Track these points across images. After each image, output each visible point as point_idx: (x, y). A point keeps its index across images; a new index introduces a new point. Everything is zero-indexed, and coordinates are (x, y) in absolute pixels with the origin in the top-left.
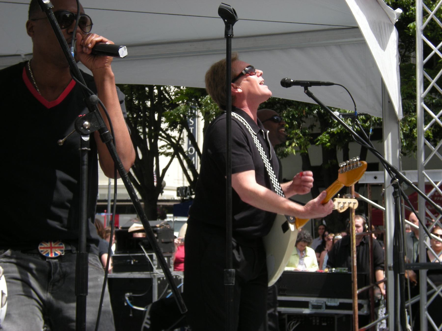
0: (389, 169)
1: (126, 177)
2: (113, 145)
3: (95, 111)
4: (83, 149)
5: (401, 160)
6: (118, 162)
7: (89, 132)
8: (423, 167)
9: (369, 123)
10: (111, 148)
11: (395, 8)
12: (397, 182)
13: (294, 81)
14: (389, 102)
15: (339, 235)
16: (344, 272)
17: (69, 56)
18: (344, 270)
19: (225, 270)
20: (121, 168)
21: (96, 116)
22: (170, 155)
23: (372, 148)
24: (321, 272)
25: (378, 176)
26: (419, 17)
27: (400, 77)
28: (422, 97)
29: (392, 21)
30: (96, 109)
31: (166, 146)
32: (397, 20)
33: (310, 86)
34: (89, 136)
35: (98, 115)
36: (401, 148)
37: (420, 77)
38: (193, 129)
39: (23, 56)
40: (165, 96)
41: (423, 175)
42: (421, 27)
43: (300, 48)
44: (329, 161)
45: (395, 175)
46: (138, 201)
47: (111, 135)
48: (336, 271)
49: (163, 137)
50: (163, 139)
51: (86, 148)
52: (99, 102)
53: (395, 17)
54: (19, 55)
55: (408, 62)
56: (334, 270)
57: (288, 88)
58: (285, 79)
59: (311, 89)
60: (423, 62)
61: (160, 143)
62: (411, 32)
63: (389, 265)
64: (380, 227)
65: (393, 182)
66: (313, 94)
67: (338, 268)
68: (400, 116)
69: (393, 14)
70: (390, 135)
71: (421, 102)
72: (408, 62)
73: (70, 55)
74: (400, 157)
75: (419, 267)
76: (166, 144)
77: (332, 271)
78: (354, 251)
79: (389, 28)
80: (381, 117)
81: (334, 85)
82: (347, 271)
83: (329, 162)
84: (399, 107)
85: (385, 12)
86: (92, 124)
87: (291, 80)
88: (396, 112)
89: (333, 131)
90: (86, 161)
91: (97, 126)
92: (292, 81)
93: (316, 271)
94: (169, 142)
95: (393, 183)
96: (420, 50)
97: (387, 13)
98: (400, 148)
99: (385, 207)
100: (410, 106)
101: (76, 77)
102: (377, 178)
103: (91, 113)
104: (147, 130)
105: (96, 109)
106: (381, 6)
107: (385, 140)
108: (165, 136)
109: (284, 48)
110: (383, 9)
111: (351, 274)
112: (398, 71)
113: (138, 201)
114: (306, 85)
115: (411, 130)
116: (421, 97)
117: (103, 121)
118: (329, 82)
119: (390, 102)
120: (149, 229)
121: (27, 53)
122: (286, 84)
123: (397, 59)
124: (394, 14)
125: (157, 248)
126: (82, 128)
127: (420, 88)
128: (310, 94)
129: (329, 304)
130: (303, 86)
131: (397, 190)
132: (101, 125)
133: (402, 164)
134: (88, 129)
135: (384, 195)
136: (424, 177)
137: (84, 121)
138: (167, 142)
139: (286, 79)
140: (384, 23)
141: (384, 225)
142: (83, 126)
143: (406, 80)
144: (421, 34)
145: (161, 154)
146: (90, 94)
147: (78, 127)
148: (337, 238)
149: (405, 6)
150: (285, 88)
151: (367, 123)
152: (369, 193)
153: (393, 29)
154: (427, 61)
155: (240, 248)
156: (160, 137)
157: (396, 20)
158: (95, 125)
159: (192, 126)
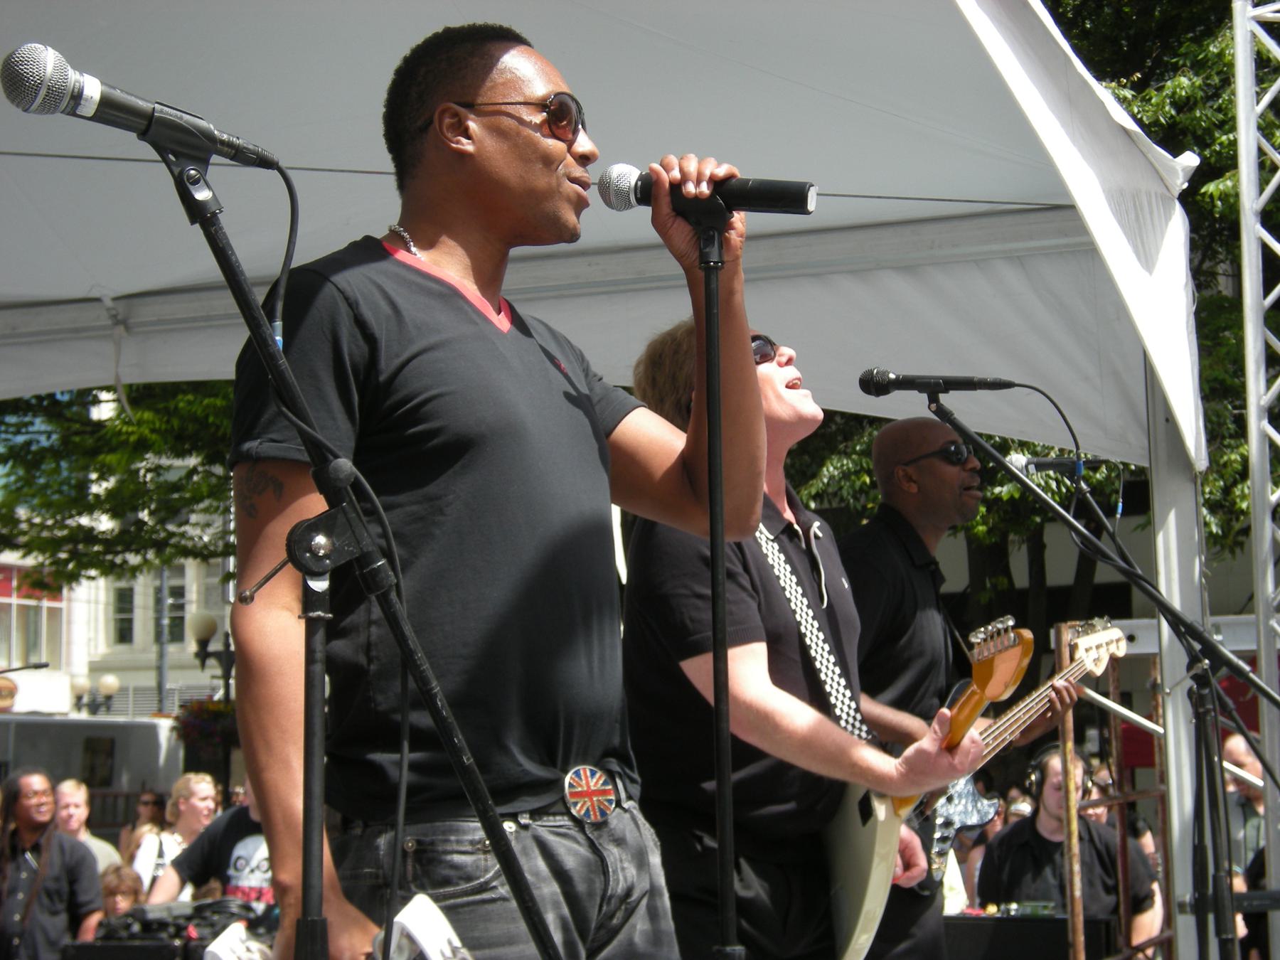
0: (1180, 630)
1: (436, 694)
2: (398, 601)
3: (345, 504)
4: (311, 614)
5: (1205, 588)
6: (411, 650)
7: (327, 565)
8: (1272, 609)
9: (1105, 471)
10: (392, 610)
11: (1176, 152)
12: (1205, 667)
13: (898, 377)
14: (1167, 420)
15: (1023, 801)
16: (1044, 915)
17: (270, 348)
18: (1045, 907)
19: (716, 948)
20: (422, 669)
21: (348, 520)
23: (1132, 569)
24: (977, 915)
25: (1138, 634)
26: (1249, 174)
27: (1198, 343)
28: (1263, 406)
29: (1170, 187)
30: (347, 499)
32: (1186, 185)
33: (946, 391)
34: (328, 576)
35: (354, 515)
36: (1205, 552)
37: (1255, 348)
39: (109, 303)
41: (1273, 634)
42: (1253, 202)
43: (907, 269)
44: (987, 581)
45: (1197, 646)
46: (471, 763)
47: (391, 573)
48: (1020, 912)
51: (320, 613)
52: (356, 485)
53: (1178, 178)
54: (98, 300)
55: (1212, 288)
56: (1014, 910)
57: (882, 397)
58: (873, 372)
59: (949, 400)
60: (1262, 304)
62: (1219, 208)
63: (1180, 899)
64: (1141, 773)
65: (1195, 668)
66: (953, 414)
67: (1027, 904)
68: (1201, 460)
69: (1173, 171)
70: (1172, 517)
71: (1260, 419)
72: (1212, 288)
73: (271, 345)
74: (1203, 580)
75: (1267, 902)
77: (1008, 911)
78: (1075, 855)
79: (1162, 210)
80: (1146, 465)
81: (1016, 388)
82: (1052, 913)
83: (988, 585)
84: (1198, 434)
85: (1151, 164)
86: (335, 542)
87: (889, 373)
88: (1188, 449)
89: (1001, 492)
90: (320, 651)
91: (351, 549)
92: (892, 376)
93: (962, 913)
95: (1193, 672)
96: (1254, 271)
97: (1157, 165)
98: (1202, 553)
99: (1164, 726)
100: (1222, 420)
101: (288, 408)
102: (1135, 642)
103: (332, 510)
105: (347, 499)
106: (1138, 147)
107: (1158, 532)
109: (862, 270)
110: (1144, 155)
111: (1064, 921)
112: (1190, 329)
113: (469, 762)
114: (933, 388)
115: (1227, 491)
116: (1258, 405)
117: (367, 532)
118: (1001, 379)
119: (1170, 420)
120: (503, 843)
121: (119, 294)
122: (873, 385)
123: (1187, 297)
124: (1177, 170)
125: (527, 898)
126: (308, 555)
127: (1257, 379)
128: (942, 413)
130: (925, 393)
131: (1206, 691)
132: (361, 546)
133: (1210, 601)
134: (326, 556)
135: (1156, 688)
136: (1274, 637)
139: (875, 371)
140: (1149, 194)
141: (1158, 767)
142: (310, 549)
143: (1209, 343)
144: (1255, 224)
147: (297, 553)
148: (1016, 810)
149: (1200, 132)
150: (873, 397)
151: (1100, 471)
152: (1113, 681)
153: (1174, 209)
154: (1275, 299)
155: (743, 862)
157: (1183, 184)
158: (346, 545)
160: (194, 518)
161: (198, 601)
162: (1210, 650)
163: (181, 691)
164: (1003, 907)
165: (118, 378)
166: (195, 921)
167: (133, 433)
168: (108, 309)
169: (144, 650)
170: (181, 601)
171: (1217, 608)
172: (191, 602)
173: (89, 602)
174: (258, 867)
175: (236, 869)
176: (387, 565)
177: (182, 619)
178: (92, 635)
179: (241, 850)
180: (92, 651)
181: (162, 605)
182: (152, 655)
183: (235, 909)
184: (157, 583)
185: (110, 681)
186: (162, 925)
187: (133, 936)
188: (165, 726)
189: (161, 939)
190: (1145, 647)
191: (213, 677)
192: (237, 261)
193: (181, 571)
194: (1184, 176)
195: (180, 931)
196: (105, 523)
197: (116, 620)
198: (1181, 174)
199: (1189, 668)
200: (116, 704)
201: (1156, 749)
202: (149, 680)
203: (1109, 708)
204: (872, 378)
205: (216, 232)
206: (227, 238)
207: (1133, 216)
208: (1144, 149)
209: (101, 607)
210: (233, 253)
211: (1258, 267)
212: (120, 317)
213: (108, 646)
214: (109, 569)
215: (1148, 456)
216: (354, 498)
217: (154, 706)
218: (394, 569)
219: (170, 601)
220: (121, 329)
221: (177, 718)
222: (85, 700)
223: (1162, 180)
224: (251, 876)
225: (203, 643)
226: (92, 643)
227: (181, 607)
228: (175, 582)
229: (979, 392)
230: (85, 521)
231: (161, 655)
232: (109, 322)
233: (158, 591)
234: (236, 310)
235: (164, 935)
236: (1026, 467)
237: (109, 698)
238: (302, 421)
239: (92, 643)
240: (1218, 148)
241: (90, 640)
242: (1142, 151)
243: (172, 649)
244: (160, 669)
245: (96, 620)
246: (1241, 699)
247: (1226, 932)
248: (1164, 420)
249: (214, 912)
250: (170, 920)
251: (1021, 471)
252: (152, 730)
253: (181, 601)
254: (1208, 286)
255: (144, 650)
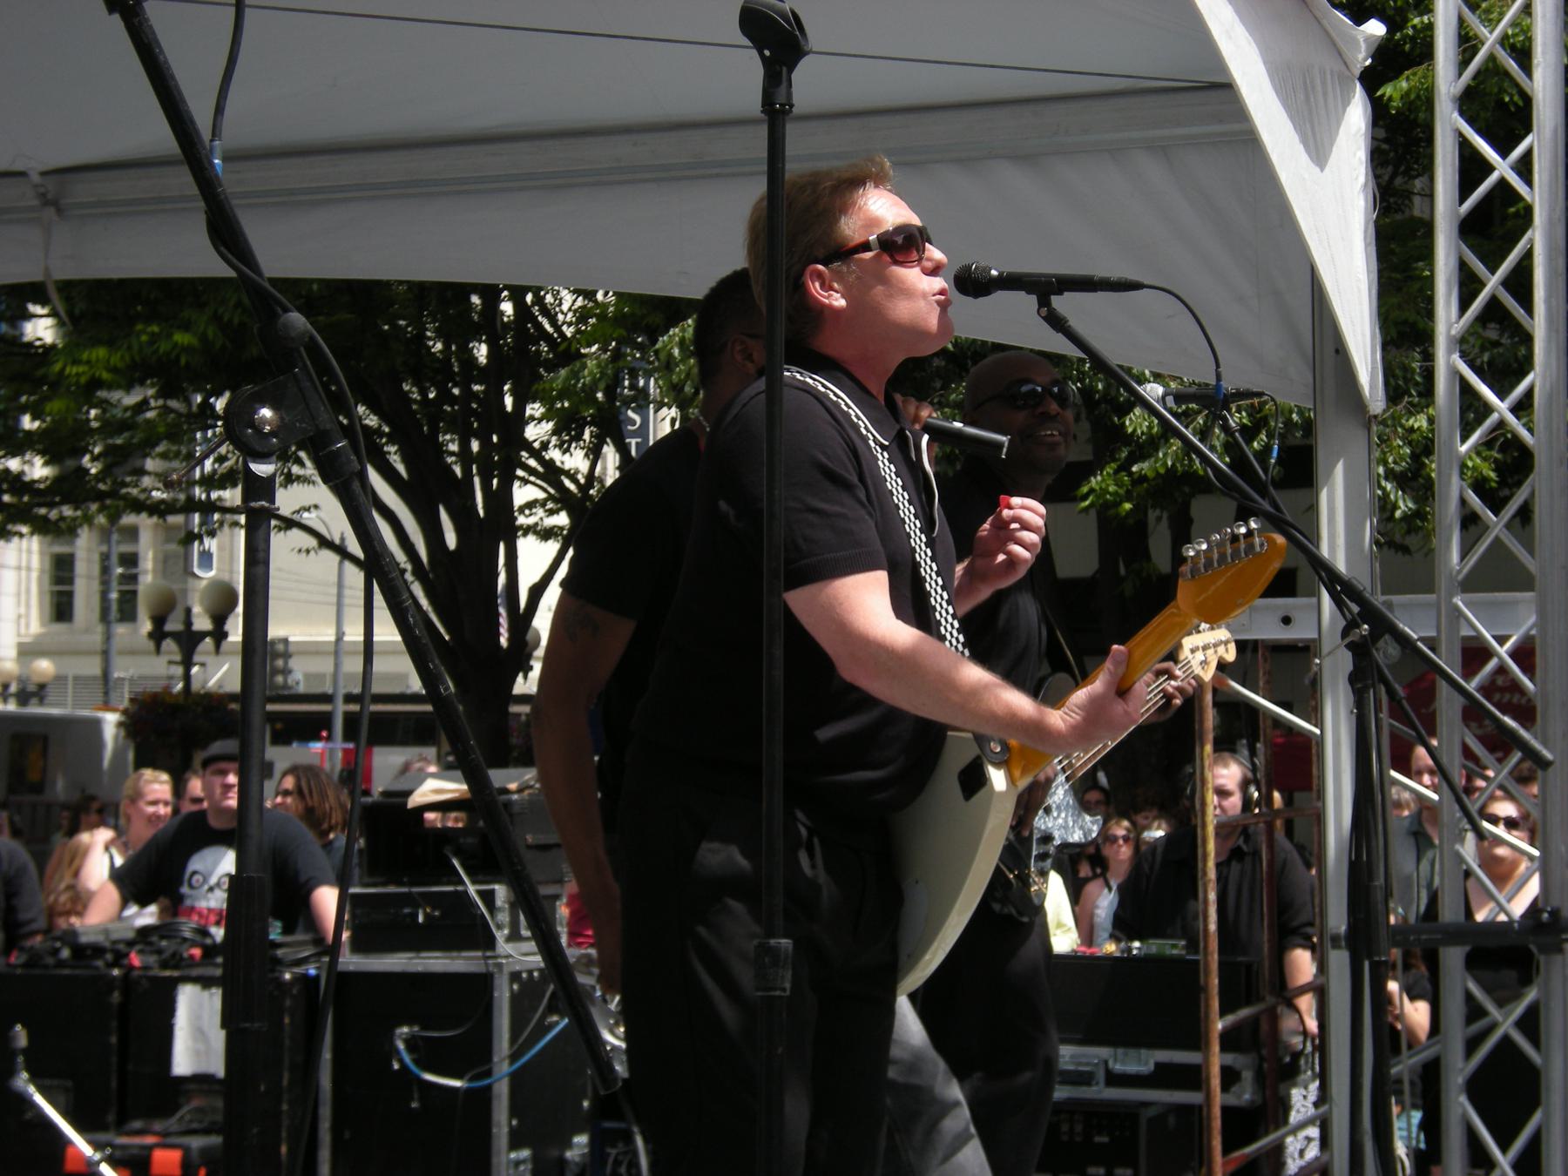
4: (253, 504)
5: (1376, 557)
7: (274, 445)
9: (1265, 439)
11: (1359, 19)
13: (1001, 274)
14: (1337, 351)
18: (1174, 946)
22: (556, 535)
25: (1293, 614)
26: (1446, 50)
28: (1454, 336)
30: (300, 364)
31: (543, 504)
33: (1060, 292)
35: (308, 384)
38: (637, 443)
39: (36, 178)
40: (539, 326)
43: (1024, 158)
45: (1355, 609)
47: (353, 457)
49: (532, 471)
50: (532, 479)
52: (312, 347)
53: (1360, 52)
54: (22, 174)
60: (1457, 212)
61: (523, 494)
63: (1334, 931)
69: (1355, 41)
71: (1450, 352)
76: (541, 495)
77: (1130, 950)
78: (1210, 880)
82: (1184, 952)
86: (284, 416)
91: (304, 425)
92: (994, 272)
93: (1073, 951)
94: (552, 491)
95: (1347, 640)
96: (1449, 170)
97: (1334, 35)
104: (475, 446)
105: (300, 364)
107: (1323, 488)
108: (540, 469)
111: (1197, 962)
114: (1045, 288)
125: (516, 860)
127: (1448, 303)
128: (1056, 322)
129: (1118, 1067)
134: (272, 434)
135: (1315, 683)
136: (1458, 617)
137: (257, 406)
138: (545, 490)
145: (525, 535)
146: (279, 310)
152: (1264, 674)
156: (520, 473)
157: (1366, 60)
159: (634, 434)
160: (150, 464)
161: (155, 571)
162: (1383, 626)
163: (131, 680)
164: (1123, 945)
165: (47, 271)
166: (138, 947)
167: (83, 373)
168: (36, 186)
169: (87, 631)
170: (134, 571)
171: (1391, 586)
172: (146, 572)
173: (19, 568)
174: (218, 885)
175: (191, 886)
176: (349, 448)
177: (134, 593)
178: (23, 610)
179: (197, 863)
180: (23, 631)
181: (110, 576)
182: (96, 638)
183: (188, 934)
184: (104, 548)
185: (45, 666)
186: (98, 950)
187: (61, 964)
188: (111, 720)
189: (97, 968)
190: (1300, 632)
191: (170, 662)
192: (166, 62)
193: (132, 533)
194: (1367, 48)
195: (119, 958)
196: (38, 470)
197: (52, 593)
198: (1363, 46)
199: (1345, 633)
200: (51, 695)
201: (1314, 759)
202: (93, 667)
203: (1258, 703)
204: (970, 275)
205: (141, 24)
206: (154, 33)
207: (1301, 96)
208: (1318, 14)
209: (35, 575)
210: (161, 51)
211: (1454, 164)
212: (50, 196)
213: (43, 624)
214: (42, 527)
215: (1312, 396)
216: (308, 363)
217: (100, 698)
218: (357, 452)
219: (120, 570)
220: (51, 211)
221: (125, 712)
222: (13, 688)
223: (1340, 54)
224: (210, 895)
225: (159, 620)
226: (23, 621)
227: (133, 579)
228: (126, 548)
229: (1100, 294)
230: (14, 464)
231: (108, 637)
232: (35, 202)
233: (105, 558)
234: (195, 191)
235: (100, 963)
236: (1164, 397)
237: (42, 687)
238: (246, 266)
239: (23, 621)
240: (1410, 32)
241: (19, 617)
242: (1315, 17)
243: (121, 630)
244: (106, 654)
245: (28, 591)
246: (1423, 711)
247: (1379, 954)
248: (1333, 350)
249: (163, 937)
250: (107, 944)
251: (1158, 402)
252: (96, 724)
253: (134, 571)
254: (1399, 210)
255: (87, 631)
